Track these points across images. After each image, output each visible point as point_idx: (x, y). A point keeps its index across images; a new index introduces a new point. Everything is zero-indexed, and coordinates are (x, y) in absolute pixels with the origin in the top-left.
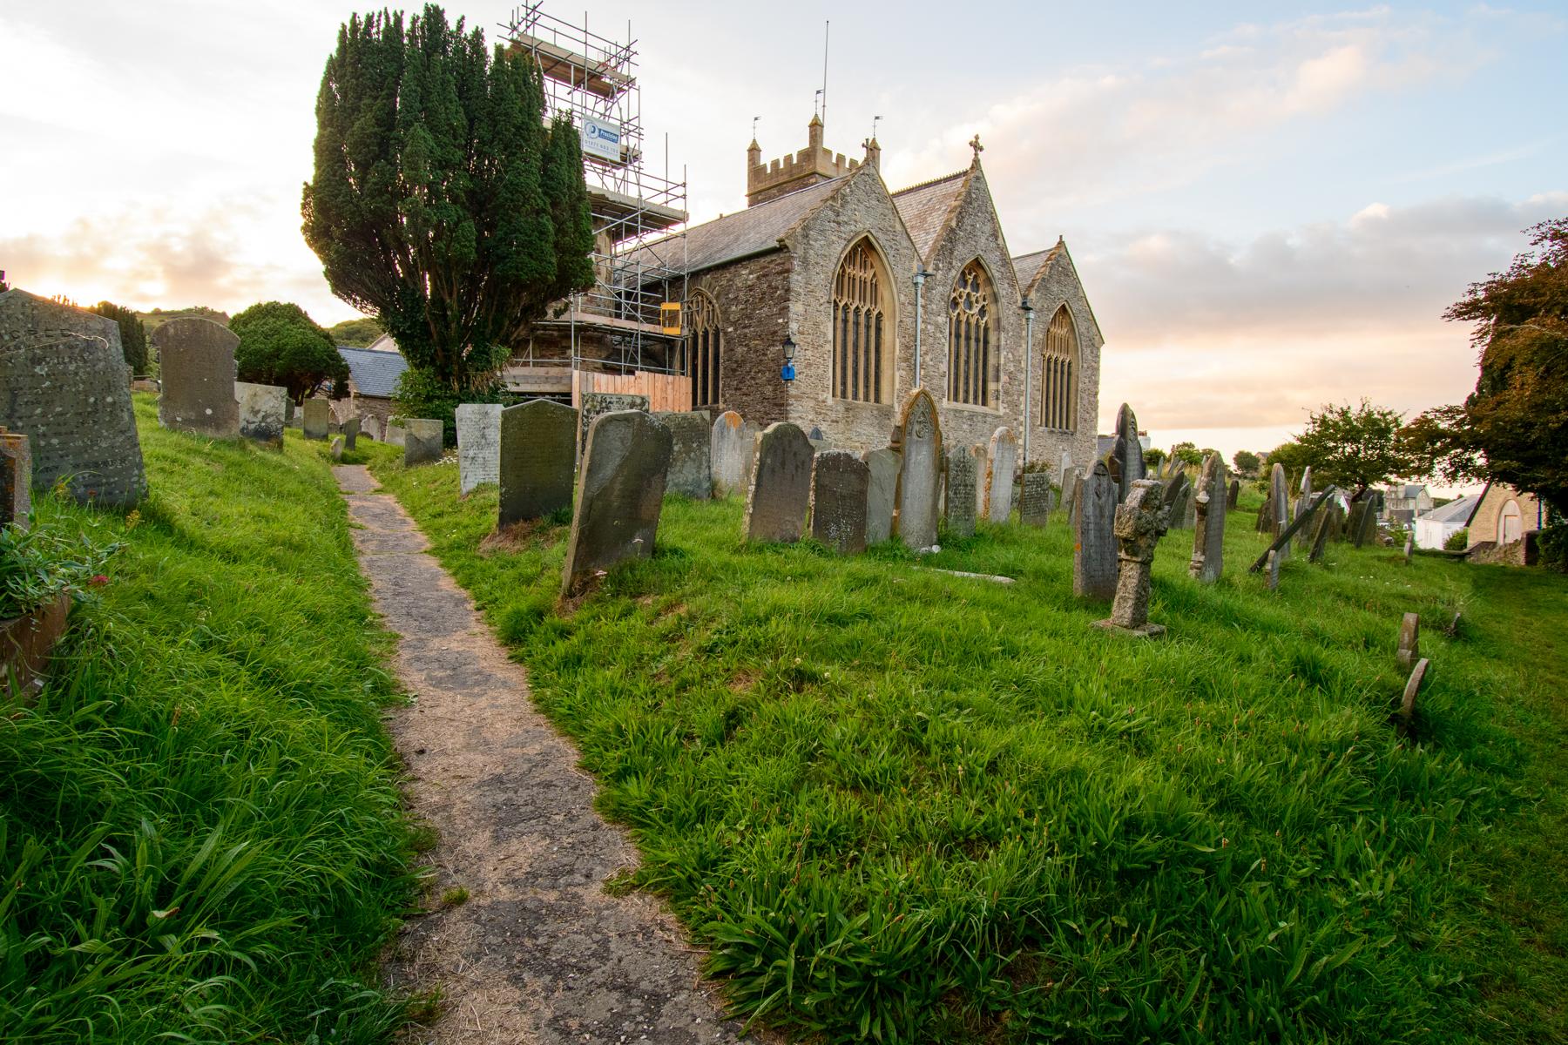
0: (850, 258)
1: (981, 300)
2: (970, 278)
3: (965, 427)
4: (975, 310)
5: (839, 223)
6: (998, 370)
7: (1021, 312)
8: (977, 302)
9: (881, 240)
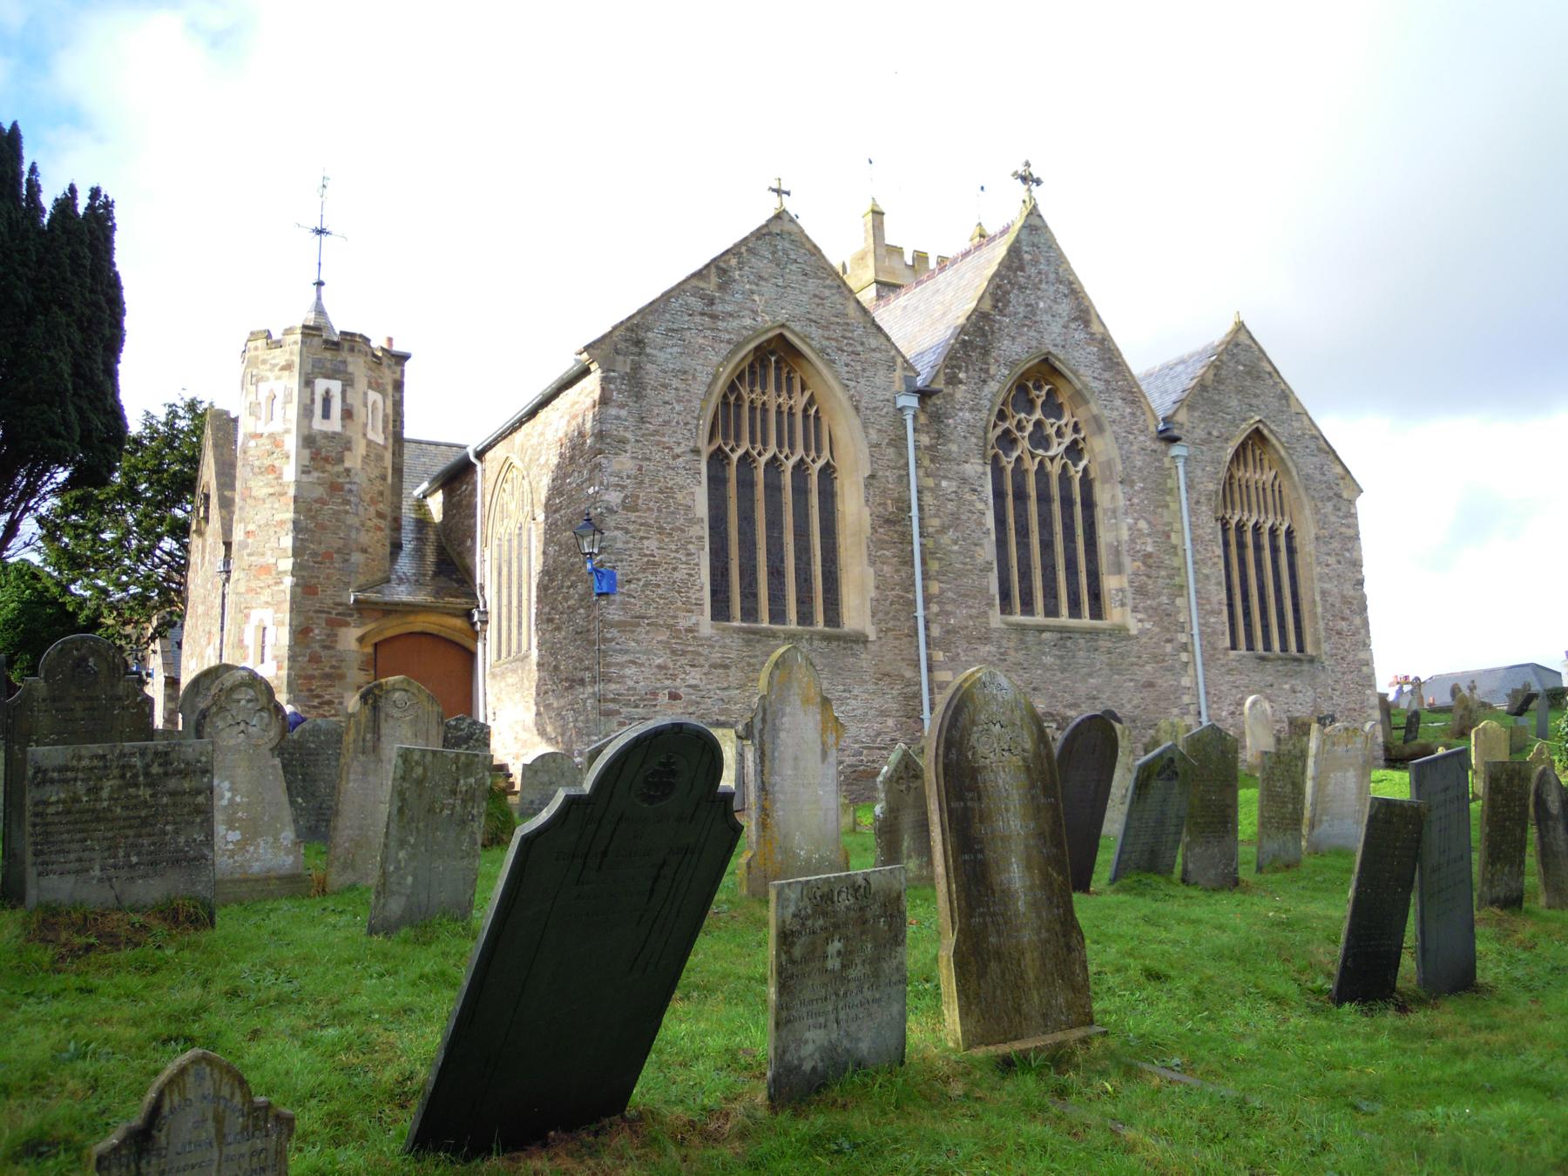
0: (1240, 455)
1: (1068, 431)
2: (1040, 396)
3: (1048, 660)
4: (1057, 449)
5: (714, 317)
6: (1117, 553)
7: (1161, 446)
8: (1059, 433)
9: (808, 337)
